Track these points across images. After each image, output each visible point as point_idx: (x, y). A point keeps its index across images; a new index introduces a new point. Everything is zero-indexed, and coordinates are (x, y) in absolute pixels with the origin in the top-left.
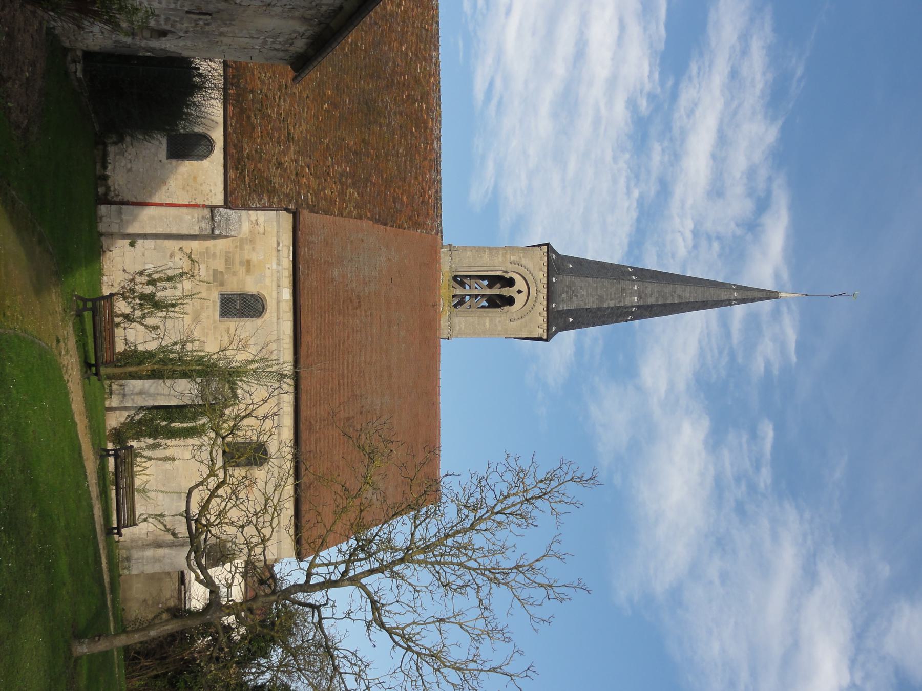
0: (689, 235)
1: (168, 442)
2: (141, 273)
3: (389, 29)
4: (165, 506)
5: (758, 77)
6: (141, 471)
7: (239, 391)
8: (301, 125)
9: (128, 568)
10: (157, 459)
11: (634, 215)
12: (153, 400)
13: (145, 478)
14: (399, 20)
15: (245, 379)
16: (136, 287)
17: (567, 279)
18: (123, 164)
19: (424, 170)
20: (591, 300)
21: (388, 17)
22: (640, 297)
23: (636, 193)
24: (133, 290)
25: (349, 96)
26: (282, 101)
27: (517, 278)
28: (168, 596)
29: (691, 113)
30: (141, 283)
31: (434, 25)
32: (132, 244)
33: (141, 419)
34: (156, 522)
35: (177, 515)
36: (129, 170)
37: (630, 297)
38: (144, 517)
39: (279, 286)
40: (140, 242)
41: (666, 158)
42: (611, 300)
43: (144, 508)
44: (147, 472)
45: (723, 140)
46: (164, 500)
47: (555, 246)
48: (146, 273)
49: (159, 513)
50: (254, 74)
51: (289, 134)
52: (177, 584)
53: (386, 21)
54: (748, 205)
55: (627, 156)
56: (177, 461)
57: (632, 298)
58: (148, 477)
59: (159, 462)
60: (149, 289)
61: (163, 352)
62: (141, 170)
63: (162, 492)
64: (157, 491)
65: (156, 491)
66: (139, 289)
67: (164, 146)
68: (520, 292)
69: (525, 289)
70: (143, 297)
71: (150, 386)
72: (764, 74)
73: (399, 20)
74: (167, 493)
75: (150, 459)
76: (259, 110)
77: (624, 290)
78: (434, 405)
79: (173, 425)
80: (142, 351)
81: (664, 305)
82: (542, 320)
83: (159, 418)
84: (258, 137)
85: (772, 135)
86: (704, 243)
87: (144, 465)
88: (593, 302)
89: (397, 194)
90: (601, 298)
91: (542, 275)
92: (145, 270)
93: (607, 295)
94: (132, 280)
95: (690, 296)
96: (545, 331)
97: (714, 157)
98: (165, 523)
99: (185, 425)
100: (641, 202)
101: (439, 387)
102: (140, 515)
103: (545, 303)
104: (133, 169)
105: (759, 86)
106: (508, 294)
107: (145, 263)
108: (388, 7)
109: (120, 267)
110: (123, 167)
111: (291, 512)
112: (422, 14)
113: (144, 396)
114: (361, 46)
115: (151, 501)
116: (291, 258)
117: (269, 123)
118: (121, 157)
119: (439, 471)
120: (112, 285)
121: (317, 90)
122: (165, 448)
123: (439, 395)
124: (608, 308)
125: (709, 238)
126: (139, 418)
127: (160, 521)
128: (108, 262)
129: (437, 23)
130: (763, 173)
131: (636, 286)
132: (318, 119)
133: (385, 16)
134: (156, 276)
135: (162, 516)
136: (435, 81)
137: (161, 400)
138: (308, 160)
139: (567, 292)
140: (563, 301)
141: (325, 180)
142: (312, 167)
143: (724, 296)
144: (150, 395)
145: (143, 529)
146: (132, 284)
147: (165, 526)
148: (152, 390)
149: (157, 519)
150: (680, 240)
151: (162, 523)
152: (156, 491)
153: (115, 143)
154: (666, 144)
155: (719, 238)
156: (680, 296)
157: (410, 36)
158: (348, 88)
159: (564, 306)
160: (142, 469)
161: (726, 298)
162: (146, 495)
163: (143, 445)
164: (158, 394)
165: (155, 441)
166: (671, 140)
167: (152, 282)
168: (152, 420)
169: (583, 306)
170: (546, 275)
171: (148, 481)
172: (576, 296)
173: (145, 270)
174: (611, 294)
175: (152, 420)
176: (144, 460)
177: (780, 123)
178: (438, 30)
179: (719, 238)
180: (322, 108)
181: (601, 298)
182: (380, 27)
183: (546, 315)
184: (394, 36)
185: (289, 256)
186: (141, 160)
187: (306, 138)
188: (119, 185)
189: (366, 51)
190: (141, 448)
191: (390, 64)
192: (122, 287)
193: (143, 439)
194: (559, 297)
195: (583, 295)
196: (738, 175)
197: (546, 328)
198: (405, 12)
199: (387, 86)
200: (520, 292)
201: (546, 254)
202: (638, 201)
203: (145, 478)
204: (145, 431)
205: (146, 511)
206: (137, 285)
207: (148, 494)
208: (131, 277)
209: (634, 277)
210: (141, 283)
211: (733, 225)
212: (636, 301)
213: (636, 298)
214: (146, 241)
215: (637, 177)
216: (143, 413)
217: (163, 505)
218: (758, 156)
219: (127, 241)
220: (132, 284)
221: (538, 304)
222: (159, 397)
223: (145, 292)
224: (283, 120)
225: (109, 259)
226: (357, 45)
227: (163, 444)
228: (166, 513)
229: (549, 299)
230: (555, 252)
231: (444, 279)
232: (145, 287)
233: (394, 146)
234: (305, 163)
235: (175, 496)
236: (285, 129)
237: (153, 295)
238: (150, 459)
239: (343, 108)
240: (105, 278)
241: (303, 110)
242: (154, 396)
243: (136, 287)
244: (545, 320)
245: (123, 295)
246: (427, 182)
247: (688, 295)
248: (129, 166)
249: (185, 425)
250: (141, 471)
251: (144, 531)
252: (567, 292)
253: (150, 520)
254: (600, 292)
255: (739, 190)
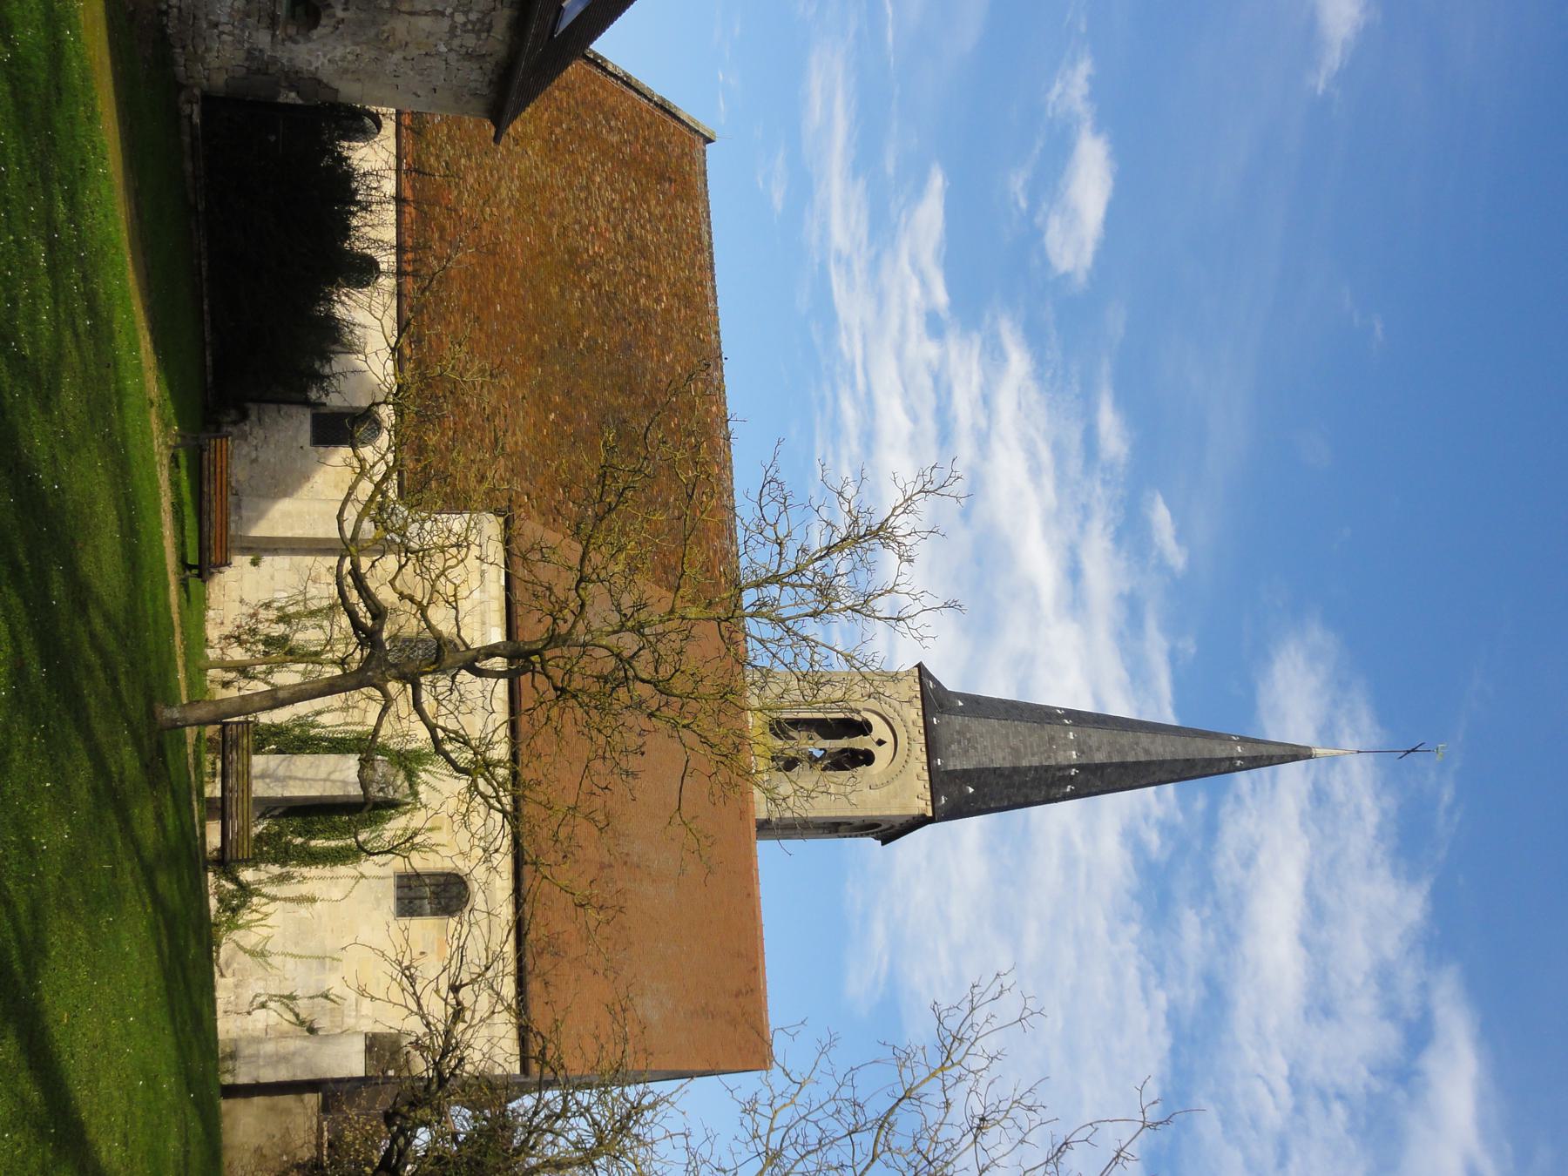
0: (1283, 1087)
1: (305, 871)
2: (267, 606)
3: (645, 330)
4: (297, 979)
5: (1367, 802)
6: (259, 920)
7: (422, 788)
8: (514, 434)
9: (232, 1072)
10: (285, 899)
11: (1165, 1041)
12: (283, 787)
13: (264, 932)
14: (659, 320)
15: (428, 767)
16: (260, 626)
17: (957, 721)
18: (244, 452)
19: (711, 534)
20: (1001, 755)
21: (642, 314)
22: (1081, 752)
23: (1161, 999)
24: (254, 630)
25: (587, 408)
26: (485, 390)
27: (874, 720)
28: (299, 1142)
29: (1248, 861)
30: (267, 620)
31: (713, 336)
32: (255, 563)
33: (261, 833)
34: (282, 1009)
35: (317, 996)
36: (255, 461)
37: (1065, 751)
38: (263, 999)
39: (483, 623)
40: (267, 560)
41: (1211, 937)
42: (1033, 755)
43: (262, 983)
44: (269, 921)
45: (1317, 913)
46: (296, 969)
47: (931, 668)
48: (275, 605)
49: (287, 993)
50: (442, 342)
51: (496, 440)
52: (315, 1120)
53: (640, 320)
54: (1389, 1037)
55: (1135, 929)
56: (318, 903)
57: (1068, 753)
58: (269, 930)
59: (289, 905)
60: (278, 630)
61: (301, 725)
62: (272, 460)
63: (293, 956)
64: (285, 954)
65: (283, 954)
66: (264, 628)
67: (307, 427)
68: (881, 743)
69: (888, 738)
70: (269, 641)
71: (279, 765)
72: (1377, 796)
73: (659, 320)
74: (300, 957)
75: (274, 899)
76: (451, 392)
77: (1052, 739)
78: (753, 915)
79: (313, 843)
80: (266, 725)
81: (1123, 765)
82: (922, 786)
83: (292, 832)
84: (450, 429)
85: (1412, 906)
86: (1313, 1105)
87: (264, 909)
88: (1004, 759)
89: (669, 561)
90: (1015, 751)
91: (914, 714)
92: (273, 601)
93: (1025, 747)
94: (254, 615)
95: (1165, 751)
96: (929, 803)
97: (1305, 941)
98: (297, 1010)
99: (333, 844)
100: (1173, 1016)
101: (757, 870)
102: (256, 996)
103: (924, 758)
104: (260, 460)
105: (1372, 819)
106: (861, 740)
107: (275, 590)
108: (642, 301)
109: (235, 595)
110: (245, 456)
111: (506, 912)
112: (694, 317)
113: (268, 780)
114: (603, 345)
115: (274, 971)
116: (503, 583)
117: (467, 415)
118: (242, 442)
119: (767, 1015)
120: (222, 623)
121: (538, 392)
122: (299, 881)
123: (758, 883)
124: (1030, 768)
125: (1322, 1096)
126: (257, 832)
127: (287, 1006)
128: (217, 588)
129: (717, 333)
130: (1408, 976)
131: (1071, 734)
132: (542, 431)
133: (638, 312)
134: (291, 610)
135: (292, 997)
136: (719, 411)
137: (294, 787)
138: (526, 484)
139: (959, 743)
140: (953, 756)
141: (554, 520)
142: (533, 496)
143: (1220, 751)
144: (277, 779)
145: (259, 1021)
146: (254, 621)
147: (297, 1015)
148: (281, 772)
149: (283, 1003)
150: (1262, 1091)
151: (291, 1010)
152: (283, 954)
153: (235, 423)
154: (1207, 911)
155: (1340, 1096)
156: (1147, 752)
157: (677, 344)
158: (586, 397)
159: (956, 764)
160: (261, 916)
161: (1224, 755)
162: (266, 962)
163: (263, 876)
164: (290, 778)
165: (284, 870)
166: (1217, 905)
167: (284, 619)
168: (279, 835)
169: (986, 763)
170: (920, 713)
171: (269, 938)
172: (975, 748)
173: (273, 601)
174: (1032, 746)
175: (279, 835)
176: (264, 900)
177: (1425, 886)
178: (719, 343)
179: (1340, 1096)
180: (547, 418)
181: (1015, 751)
182: (630, 324)
183: (927, 778)
184: (652, 340)
185: (499, 576)
186: (273, 446)
187: (522, 452)
188: (237, 481)
189: (610, 352)
190: (260, 882)
191: (649, 377)
192: (238, 627)
193: (263, 866)
194: (946, 749)
195: (985, 747)
196: (1358, 979)
197: (929, 798)
198: (667, 311)
199: (645, 406)
200: (881, 743)
201: (917, 680)
202: (1168, 1017)
203: (264, 932)
204: (268, 852)
205: (265, 989)
206: (261, 622)
207: (269, 960)
208: (252, 611)
209: (1066, 721)
210: (267, 620)
211: (1363, 1073)
212: (1075, 757)
213: (1074, 753)
214: (276, 558)
215: (1160, 969)
216: (265, 823)
217: (294, 979)
218: (1391, 946)
219: (249, 558)
220: (254, 621)
221: (912, 759)
222: (291, 783)
223: (273, 634)
224: (488, 418)
225: (218, 584)
226: (596, 342)
227: (295, 874)
228: (299, 993)
229: (931, 750)
230: (931, 677)
231: (754, 722)
232: (273, 625)
233: (661, 491)
234: (522, 488)
235: (315, 963)
236: (490, 431)
237: (284, 639)
238: (274, 899)
239: (579, 424)
240: (211, 613)
241: (518, 414)
242: (283, 780)
243: (260, 626)
244: (927, 786)
245: (238, 638)
246: (715, 552)
247: (1161, 750)
248: (254, 455)
249: (333, 844)
250: (259, 920)
251: (261, 1025)
252: (959, 743)
253: (271, 1004)
254: (1013, 742)
255: (1366, 1004)
